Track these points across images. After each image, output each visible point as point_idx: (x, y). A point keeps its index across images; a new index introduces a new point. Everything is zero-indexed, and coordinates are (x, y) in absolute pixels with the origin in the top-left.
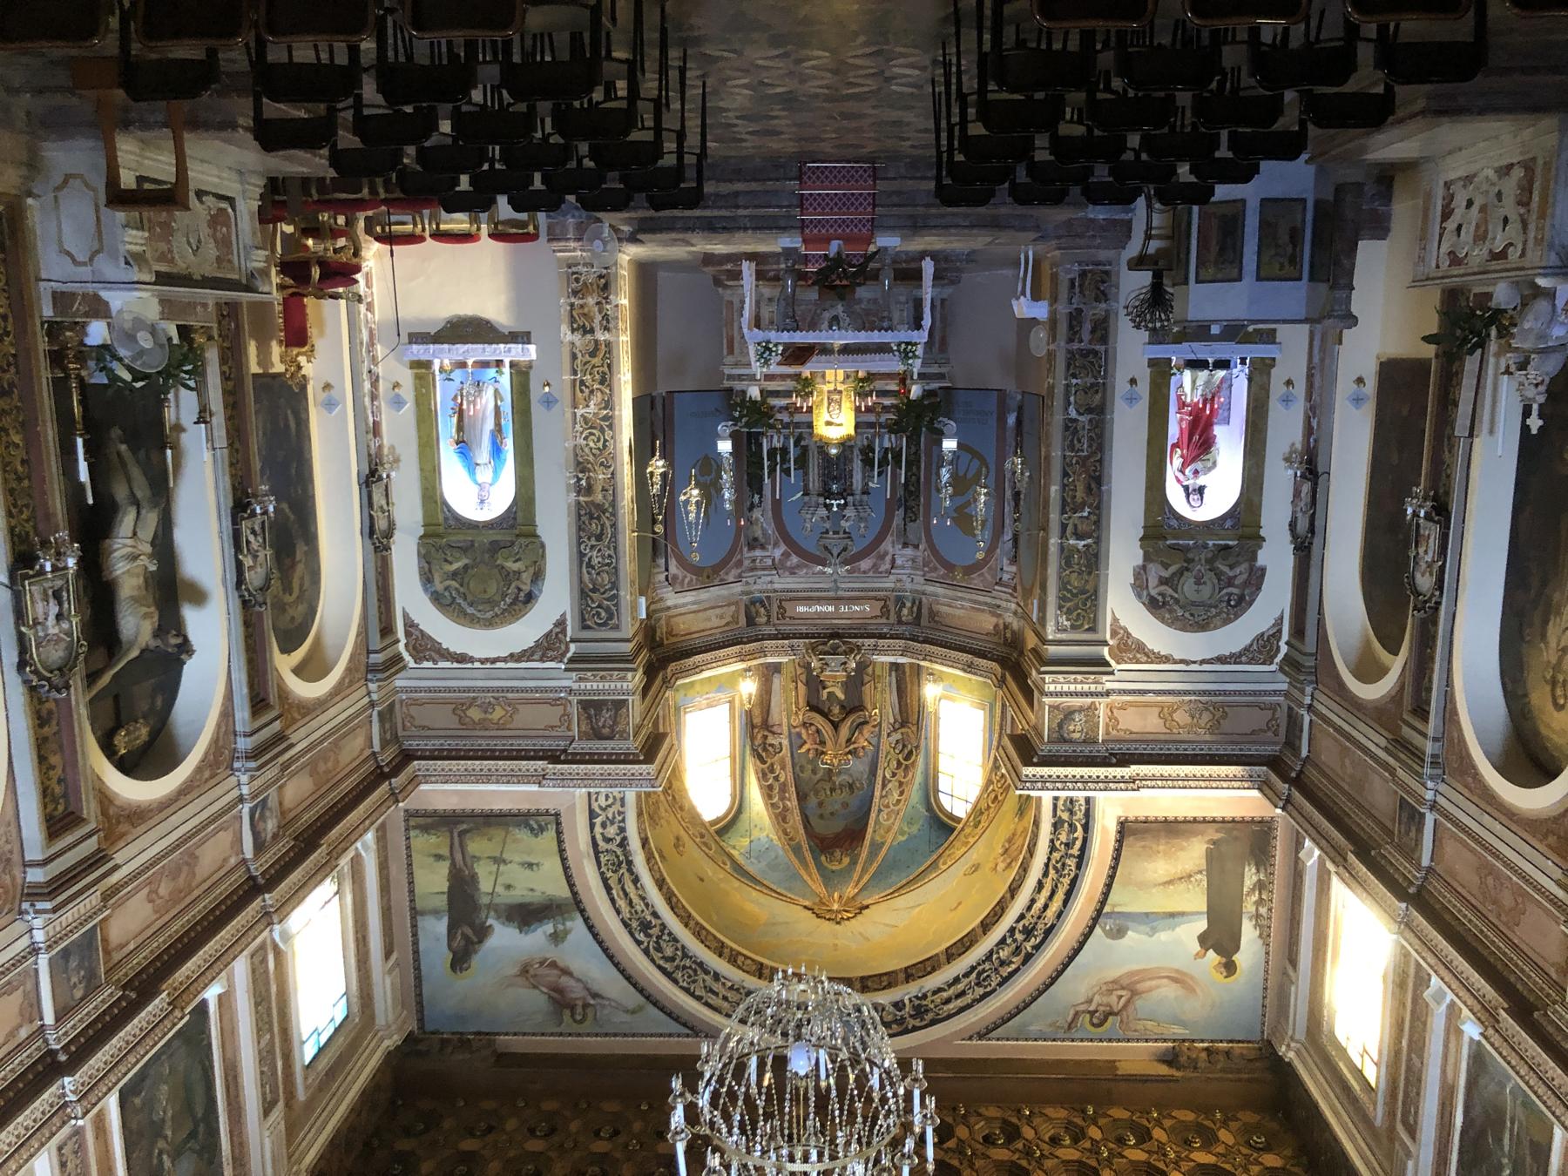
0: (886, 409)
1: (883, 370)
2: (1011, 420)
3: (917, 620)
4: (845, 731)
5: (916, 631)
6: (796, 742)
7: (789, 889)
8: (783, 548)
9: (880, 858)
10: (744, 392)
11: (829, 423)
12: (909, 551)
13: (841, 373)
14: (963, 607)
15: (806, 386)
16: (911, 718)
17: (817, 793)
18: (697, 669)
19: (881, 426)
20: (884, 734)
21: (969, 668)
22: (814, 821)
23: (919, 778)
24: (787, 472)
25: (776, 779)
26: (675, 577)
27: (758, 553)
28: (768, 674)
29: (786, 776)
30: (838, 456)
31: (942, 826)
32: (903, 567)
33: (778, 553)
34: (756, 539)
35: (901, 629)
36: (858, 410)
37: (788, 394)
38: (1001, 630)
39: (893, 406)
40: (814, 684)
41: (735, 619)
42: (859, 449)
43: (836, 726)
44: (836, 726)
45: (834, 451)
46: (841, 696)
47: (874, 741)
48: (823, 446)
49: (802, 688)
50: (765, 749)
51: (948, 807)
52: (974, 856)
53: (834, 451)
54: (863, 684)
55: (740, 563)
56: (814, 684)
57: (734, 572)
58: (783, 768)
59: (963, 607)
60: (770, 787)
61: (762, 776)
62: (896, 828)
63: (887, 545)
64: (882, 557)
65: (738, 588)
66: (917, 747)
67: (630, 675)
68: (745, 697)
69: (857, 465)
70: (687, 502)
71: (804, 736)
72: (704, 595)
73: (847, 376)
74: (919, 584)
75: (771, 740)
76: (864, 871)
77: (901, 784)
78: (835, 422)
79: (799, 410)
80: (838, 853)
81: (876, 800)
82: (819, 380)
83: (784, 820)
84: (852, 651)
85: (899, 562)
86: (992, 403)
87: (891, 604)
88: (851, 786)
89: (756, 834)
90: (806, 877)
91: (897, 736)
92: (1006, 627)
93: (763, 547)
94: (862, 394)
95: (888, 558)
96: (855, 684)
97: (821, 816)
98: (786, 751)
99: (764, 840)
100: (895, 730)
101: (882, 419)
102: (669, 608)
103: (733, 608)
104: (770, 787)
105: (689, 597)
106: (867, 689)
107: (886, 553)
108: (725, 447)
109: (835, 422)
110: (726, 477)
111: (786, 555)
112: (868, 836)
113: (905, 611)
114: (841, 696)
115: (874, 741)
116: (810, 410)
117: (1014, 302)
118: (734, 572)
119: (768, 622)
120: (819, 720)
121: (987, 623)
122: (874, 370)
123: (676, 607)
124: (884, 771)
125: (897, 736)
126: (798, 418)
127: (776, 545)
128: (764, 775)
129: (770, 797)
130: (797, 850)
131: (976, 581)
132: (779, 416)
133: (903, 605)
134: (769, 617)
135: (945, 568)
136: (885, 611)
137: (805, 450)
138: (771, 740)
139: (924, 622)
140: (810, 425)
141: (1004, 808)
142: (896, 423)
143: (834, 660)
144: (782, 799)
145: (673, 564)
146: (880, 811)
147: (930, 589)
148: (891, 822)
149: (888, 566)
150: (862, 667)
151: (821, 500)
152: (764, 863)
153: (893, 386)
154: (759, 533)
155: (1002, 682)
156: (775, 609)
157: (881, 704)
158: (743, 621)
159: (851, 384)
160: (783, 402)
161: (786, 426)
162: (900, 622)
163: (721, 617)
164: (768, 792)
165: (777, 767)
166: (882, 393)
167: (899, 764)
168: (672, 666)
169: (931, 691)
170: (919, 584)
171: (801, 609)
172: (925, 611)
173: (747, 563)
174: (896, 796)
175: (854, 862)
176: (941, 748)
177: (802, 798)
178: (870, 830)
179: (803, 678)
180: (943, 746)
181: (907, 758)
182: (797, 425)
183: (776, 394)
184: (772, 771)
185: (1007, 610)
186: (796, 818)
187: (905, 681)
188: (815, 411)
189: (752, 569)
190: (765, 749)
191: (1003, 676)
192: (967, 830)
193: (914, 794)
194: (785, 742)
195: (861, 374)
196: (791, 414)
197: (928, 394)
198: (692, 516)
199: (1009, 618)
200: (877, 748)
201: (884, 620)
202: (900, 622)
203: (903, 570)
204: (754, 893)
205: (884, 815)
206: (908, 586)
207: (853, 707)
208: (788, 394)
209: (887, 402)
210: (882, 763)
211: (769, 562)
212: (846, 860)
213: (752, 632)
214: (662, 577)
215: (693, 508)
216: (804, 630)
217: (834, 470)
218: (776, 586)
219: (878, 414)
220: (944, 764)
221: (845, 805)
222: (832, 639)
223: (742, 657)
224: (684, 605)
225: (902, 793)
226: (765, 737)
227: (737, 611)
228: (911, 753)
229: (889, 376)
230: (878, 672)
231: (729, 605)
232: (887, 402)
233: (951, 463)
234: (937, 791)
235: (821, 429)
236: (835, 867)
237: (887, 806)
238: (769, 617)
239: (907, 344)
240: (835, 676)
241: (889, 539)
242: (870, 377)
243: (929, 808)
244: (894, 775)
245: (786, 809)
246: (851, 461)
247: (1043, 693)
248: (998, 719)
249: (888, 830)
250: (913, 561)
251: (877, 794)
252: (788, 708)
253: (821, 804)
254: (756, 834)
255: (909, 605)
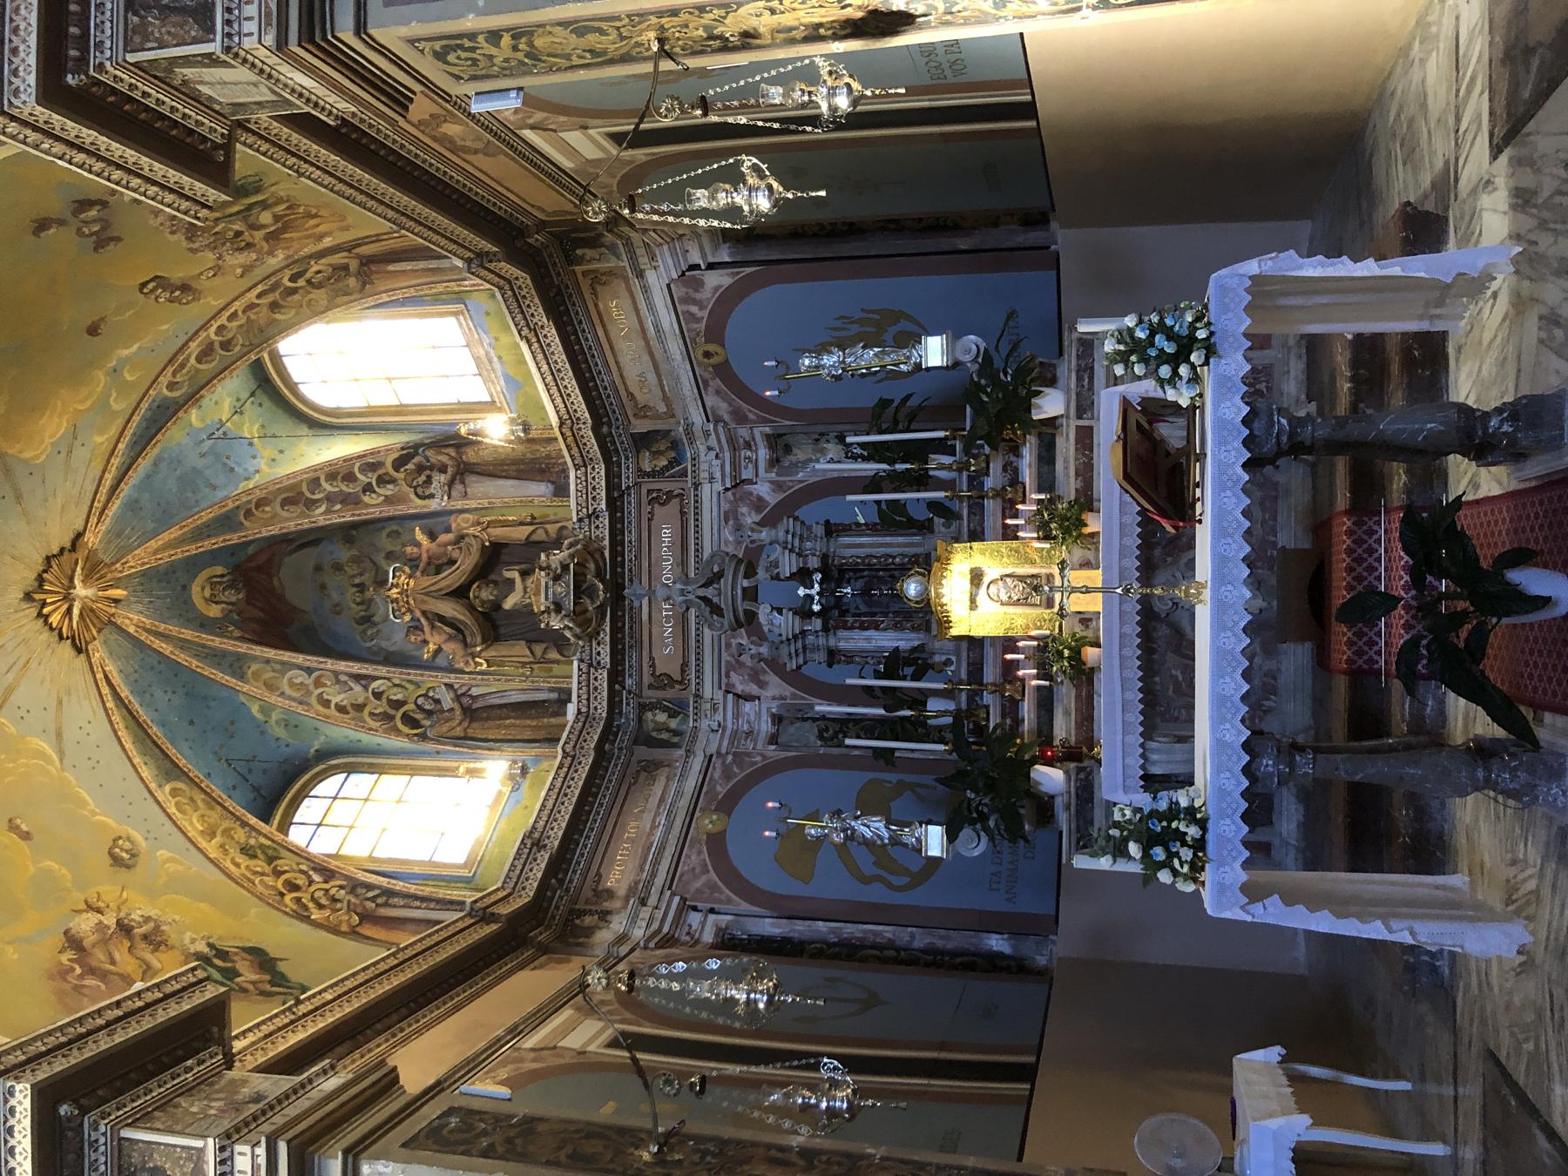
0: (1011, 708)
1: (1101, 705)
2: (997, 943)
3: (643, 739)
4: (449, 609)
5: (624, 739)
6: (434, 523)
7: (132, 506)
8: (772, 499)
9: (207, 671)
10: (1052, 382)
11: (976, 577)
12: (766, 726)
13: (1094, 603)
14: (654, 827)
15: (1065, 522)
16: (474, 724)
17: (355, 560)
18: (531, 333)
19: (973, 696)
20: (451, 679)
21: (533, 842)
22: (308, 557)
23: (367, 739)
24: (873, 484)
25: (368, 488)
26: (698, 284)
27: (763, 453)
28: (527, 464)
29: (374, 506)
30: (900, 597)
31: (276, 786)
32: (736, 716)
33: (762, 489)
34: (788, 449)
35: (629, 709)
36: (1009, 643)
37: (1046, 482)
38: (598, 903)
39: (1018, 722)
40: (527, 554)
41: (643, 411)
42: (925, 642)
43: (460, 593)
44: (460, 593)
45: (912, 588)
46: (508, 604)
47: (440, 661)
48: (927, 564)
49: (521, 533)
50: (420, 469)
51: (320, 789)
52: (166, 856)
53: (912, 588)
54: (530, 642)
55: (741, 418)
56: (527, 554)
57: (723, 409)
58: (388, 500)
59: (654, 827)
60: (350, 477)
61: (370, 463)
62: (273, 699)
63: (776, 687)
64: (755, 677)
65: (697, 417)
66: (423, 737)
67: (270, 39)
68: (480, 424)
69: (887, 640)
70: (735, 178)
71: (444, 538)
72: (675, 348)
73: (1085, 619)
74: (708, 743)
75: (440, 479)
76: (184, 644)
77: (359, 708)
78: (979, 592)
79: (1010, 509)
80: (231, 596)
81: (330, 664)
82: (1078, 553)
83: (286, 502)
84: (584, 624)
85: (748, 707)
86: (1030, 903)
87: (675, 694)
88: (367, 620)
89: (266, 451)
90: (166, 537)
91: (447, 701)
92: (604, 916)
93: (774, 462)
94: (1044, 652)
95: (753, 689)
96: (525, 627)
97: (318, 568)
98: (417, 505)
99: (251, 465)
100: (458, 698)
101: (988, 698)
102: (640, 274)
103: (662, 408)
104: (350, 477)
105: (667, 319)
106: (520, 650)
107: (762, 685)
108: (934, 351)
109: (979, 592)
110: (868, 357)
111: (759, 504)
112: (258, 651)
113: (662, 717)
114: (508, 604)
115: (440, 661)
116: (1009, 534)
117: (1274, 1053)
118: (723, 409)
119: (641, 473)
120: (467, 562)
121: (618, 877)
122: (1102, 684)
123: (646, 289)
124: (386, 678)
125: (447, 701)
126: (992, 506)
127: (778, 486)
128: (373, 467)
129: (332, 477)
130: (226, 522)
131: (695, 857)
132: (996, 467)
133: (673, 715)
134: (652, 474)
135: (732, 789)
136: (663, 681)
137: (925, 527)
138: (440, 479)
139: (642, 752)
140: (976, 535)
141: (256, 910)
142: (980, 730)
143: (565, 589)
144: (330, 498)
145: (716, 280)
146: (309, 671)
147: (697, 763)
148: (286, 691)
149: (739, 688)
150: (558, 641)
151: (814, 563)
152: (200, 463)
153: (1063, 728)
154: (800, 454)
155: (482, 915)
156: (666, 486)
157: (501, 675)
158: (641, 426)
159: (1070, 627)
160: (1028, 475)
161: (976, 481)
162: (643, 708)
163: (643, 382)
164: (340, 472)
165: (389, 490)
166: (1046, 701)
167: (397, 705)
168: (523, 279)
169: (496, 768)
170: (708, 743)
171: (667, 534)
172: (658, 754)
173: (743, 432)
174: (335, 700)
175: (204, 624)
176: (419, 781)
177: (348, 533)
178: (271, 653)
179: (540, 535)
180: (424, 785)
181: (409, 720)
182: (977, 508)
183: (1047, 457)
184: (382, 481)
185: (634, 919)
186: (293, 522)
187: (525, 722)
188: (1004, 546)
189: (732, 442)
190: (420, 469)
191: (493, 918)
192: (240, 834)
193: (341, 732)
194: (433, 505)
195: (1090, 654)
196: (999, 493)
197: (1044, 807)
198: (701, 198)
199: (618, 924)
200: (429, 666)
201: (647, 679)
202: (643, 708)
203: (733, 712)
204: (102, 440)
205: (301, 677)
206: (705, 724)
207: (494, 626)
208: (1046, 482)
209: (1028, 710)
210: (397, 674)
211: (747, 474)
212: (214, 611)
213: (622, 442)
214: (695, 258)
215: (723, 199)
216: (630, 537)
217: (874, 589)
218: (706, 489)
219: (998, 689)
220: (391, 784)
221: (337, 609)
222: (606, 587)
223: (568, 421)
224: (651, 308)
225: (341, 709)
226: (443, 470)
227: (658, 417)
228: (414, 723)
229: (1086, 717)
230: (557, 669)
231: (665, 398)
232: (1028, 710)
233: (896, 841)
234: (350, 769)
235: (961, 562)
236: (198, 592)
237: (318, 683)
238: (652, 474)
239: (1200, 845)
240: (530, 592)
241: (788, 690)
242: (1084, 676)
243: (323, 755)
244: (378, 695)
245: (311, 504)
246: (897, 627)
247: (1106, 590)
248: (442, 893)
249: (270, 687)
250: (749, 733)
251: (342, 666)
252: (506, 505)
253: (338, 567)
254: (266, 451)
255: (673, 724)
